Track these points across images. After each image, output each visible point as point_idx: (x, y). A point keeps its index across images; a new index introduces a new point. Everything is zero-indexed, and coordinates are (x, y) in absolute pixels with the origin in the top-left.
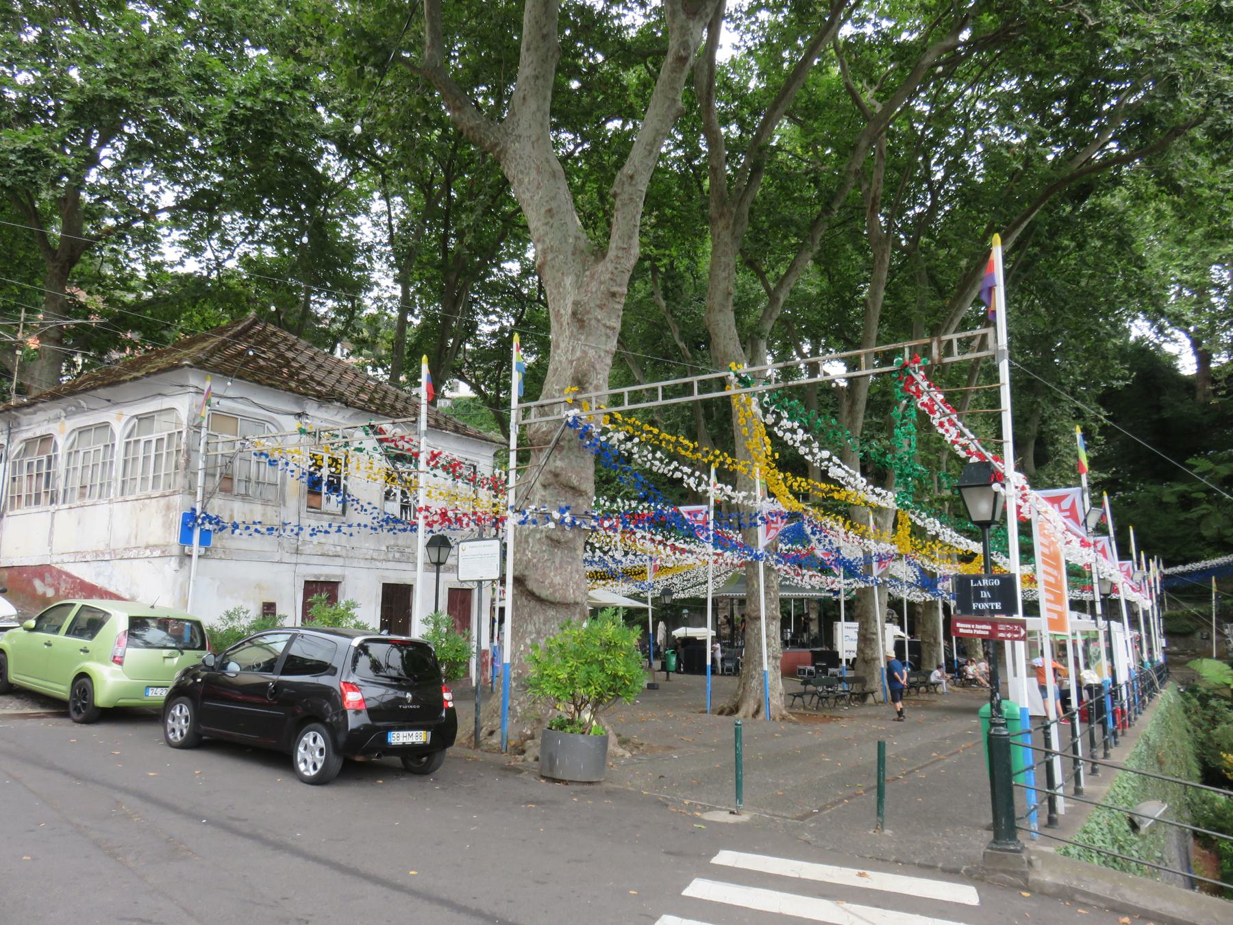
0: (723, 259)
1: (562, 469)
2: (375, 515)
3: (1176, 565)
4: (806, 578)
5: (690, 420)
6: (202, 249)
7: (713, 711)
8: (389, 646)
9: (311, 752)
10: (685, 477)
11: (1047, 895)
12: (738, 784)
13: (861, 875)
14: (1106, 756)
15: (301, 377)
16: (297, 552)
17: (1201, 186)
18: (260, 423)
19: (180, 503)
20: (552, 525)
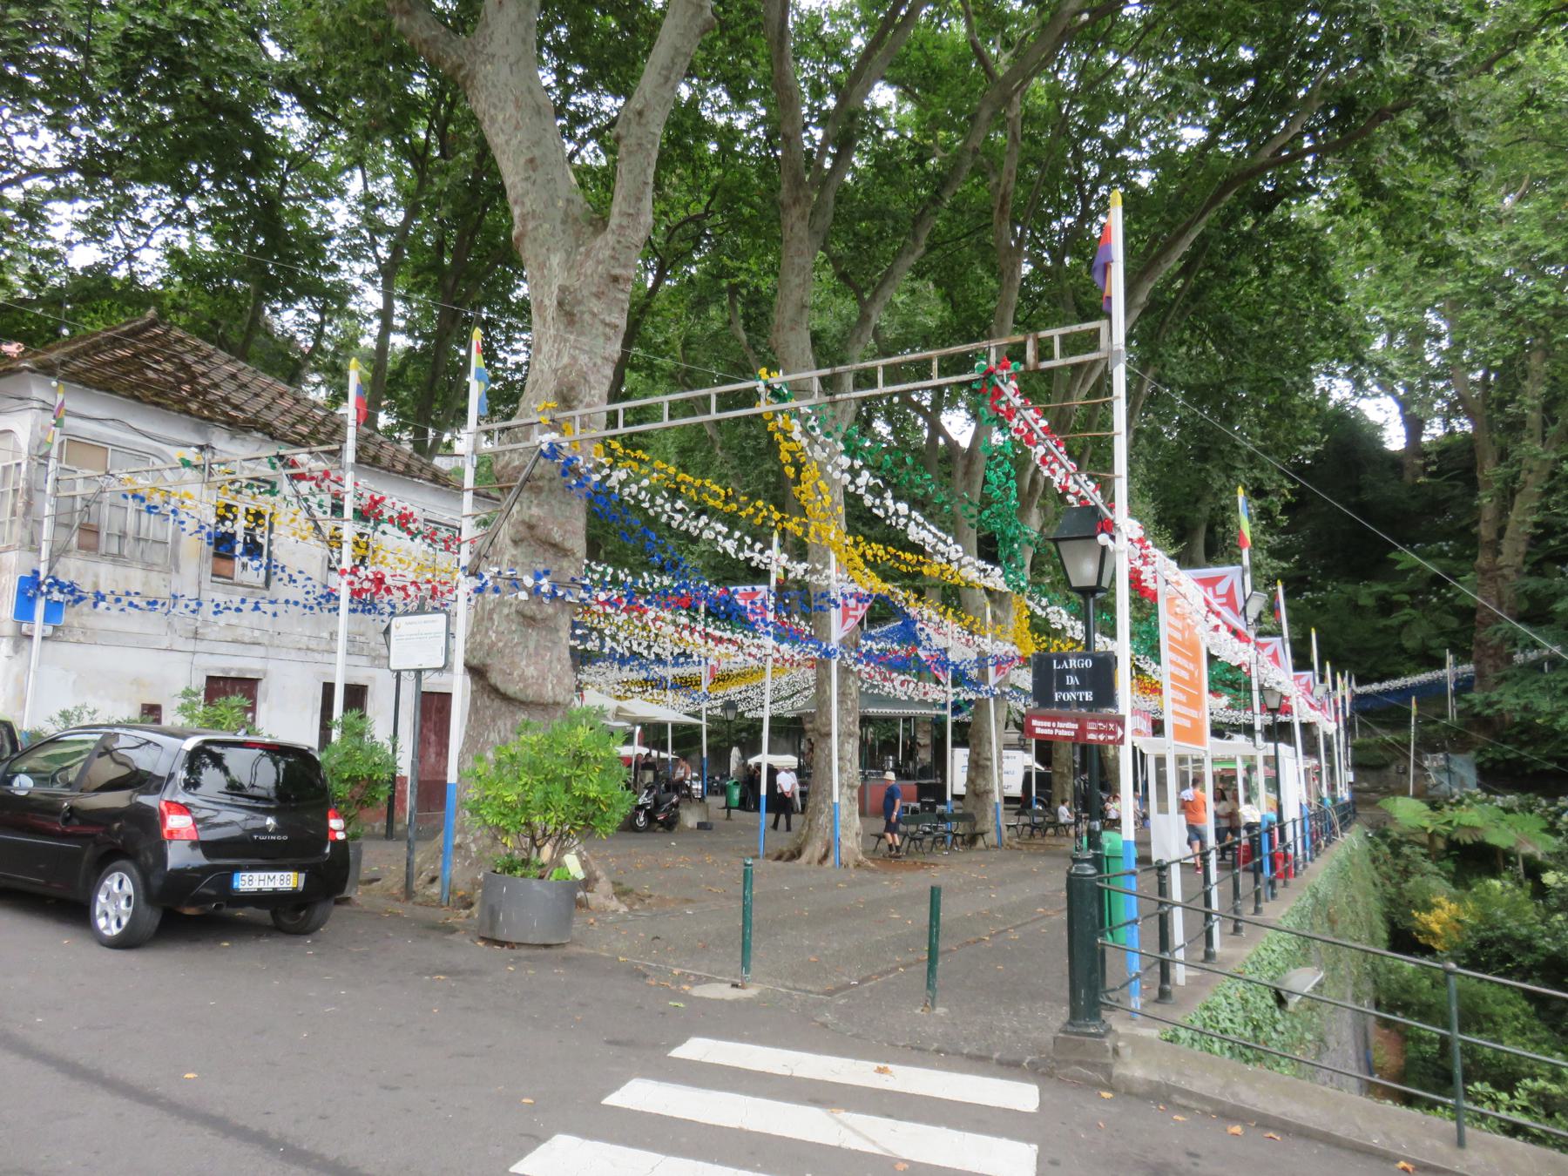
0: (797, 260)
1: (540, 518)
2: (310, 588)
3: (1370, 682)
4: (897, 683)
5: (776, 489)
6: (107, 235)
7: (767, 856)
8: (258, 752)
9: (115, 901)
10: (720, 538)
11: (1137, 1095)
12: (746, 948)
13: (880, 1071)
14: (1257, 911)
15: (210, 397)
16: (196, 636)
17: (1410, 187)
18: (143, 456)
19: (16, 564)
20: (523, 596)
